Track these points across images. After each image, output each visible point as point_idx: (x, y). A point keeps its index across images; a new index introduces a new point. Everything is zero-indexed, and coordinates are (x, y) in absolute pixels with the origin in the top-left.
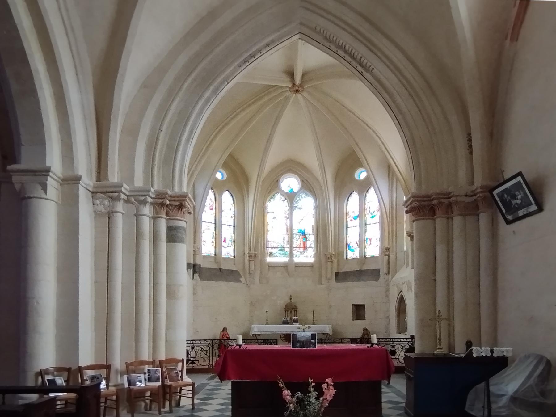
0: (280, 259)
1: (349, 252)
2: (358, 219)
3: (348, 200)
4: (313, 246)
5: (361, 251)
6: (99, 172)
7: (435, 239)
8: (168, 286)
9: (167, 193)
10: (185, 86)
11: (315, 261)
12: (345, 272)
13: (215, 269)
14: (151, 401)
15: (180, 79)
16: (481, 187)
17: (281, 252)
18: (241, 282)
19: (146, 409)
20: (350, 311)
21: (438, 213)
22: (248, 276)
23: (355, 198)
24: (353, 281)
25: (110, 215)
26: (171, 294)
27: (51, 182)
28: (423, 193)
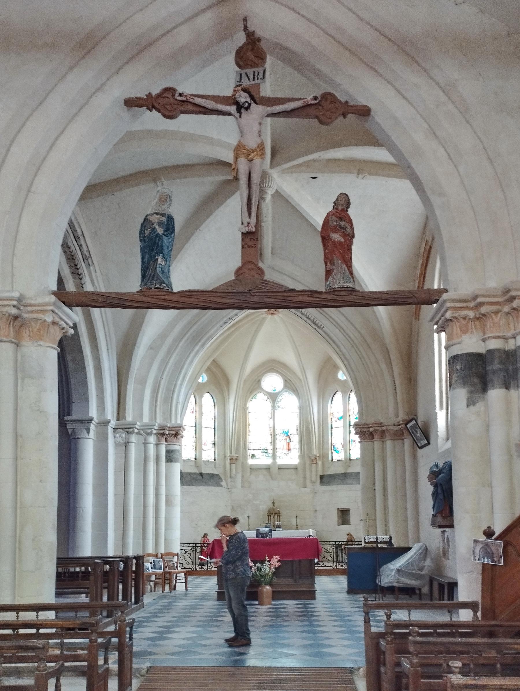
0: (264, 460)
1: (334, 453)
2: (342, 420)
3: (332, 400)
4: (298, 446)
5: (345, 452)
6: (118, 413)
7: (374, 456)
8: (167, 496)
10: (180, 345)
11: (300, 463)
13: (195, 474)
14: (156, 584)
17: (264, 454)
18: (221, 486)
19: (151, 591)
20: (335, 516)
21: (376, 437)
22: (229, 480)
23: (339, 396)
24: (338, 485)
25: (126, 444)
26: (169, 502)
27: (92, 427)
28: (363, 422)
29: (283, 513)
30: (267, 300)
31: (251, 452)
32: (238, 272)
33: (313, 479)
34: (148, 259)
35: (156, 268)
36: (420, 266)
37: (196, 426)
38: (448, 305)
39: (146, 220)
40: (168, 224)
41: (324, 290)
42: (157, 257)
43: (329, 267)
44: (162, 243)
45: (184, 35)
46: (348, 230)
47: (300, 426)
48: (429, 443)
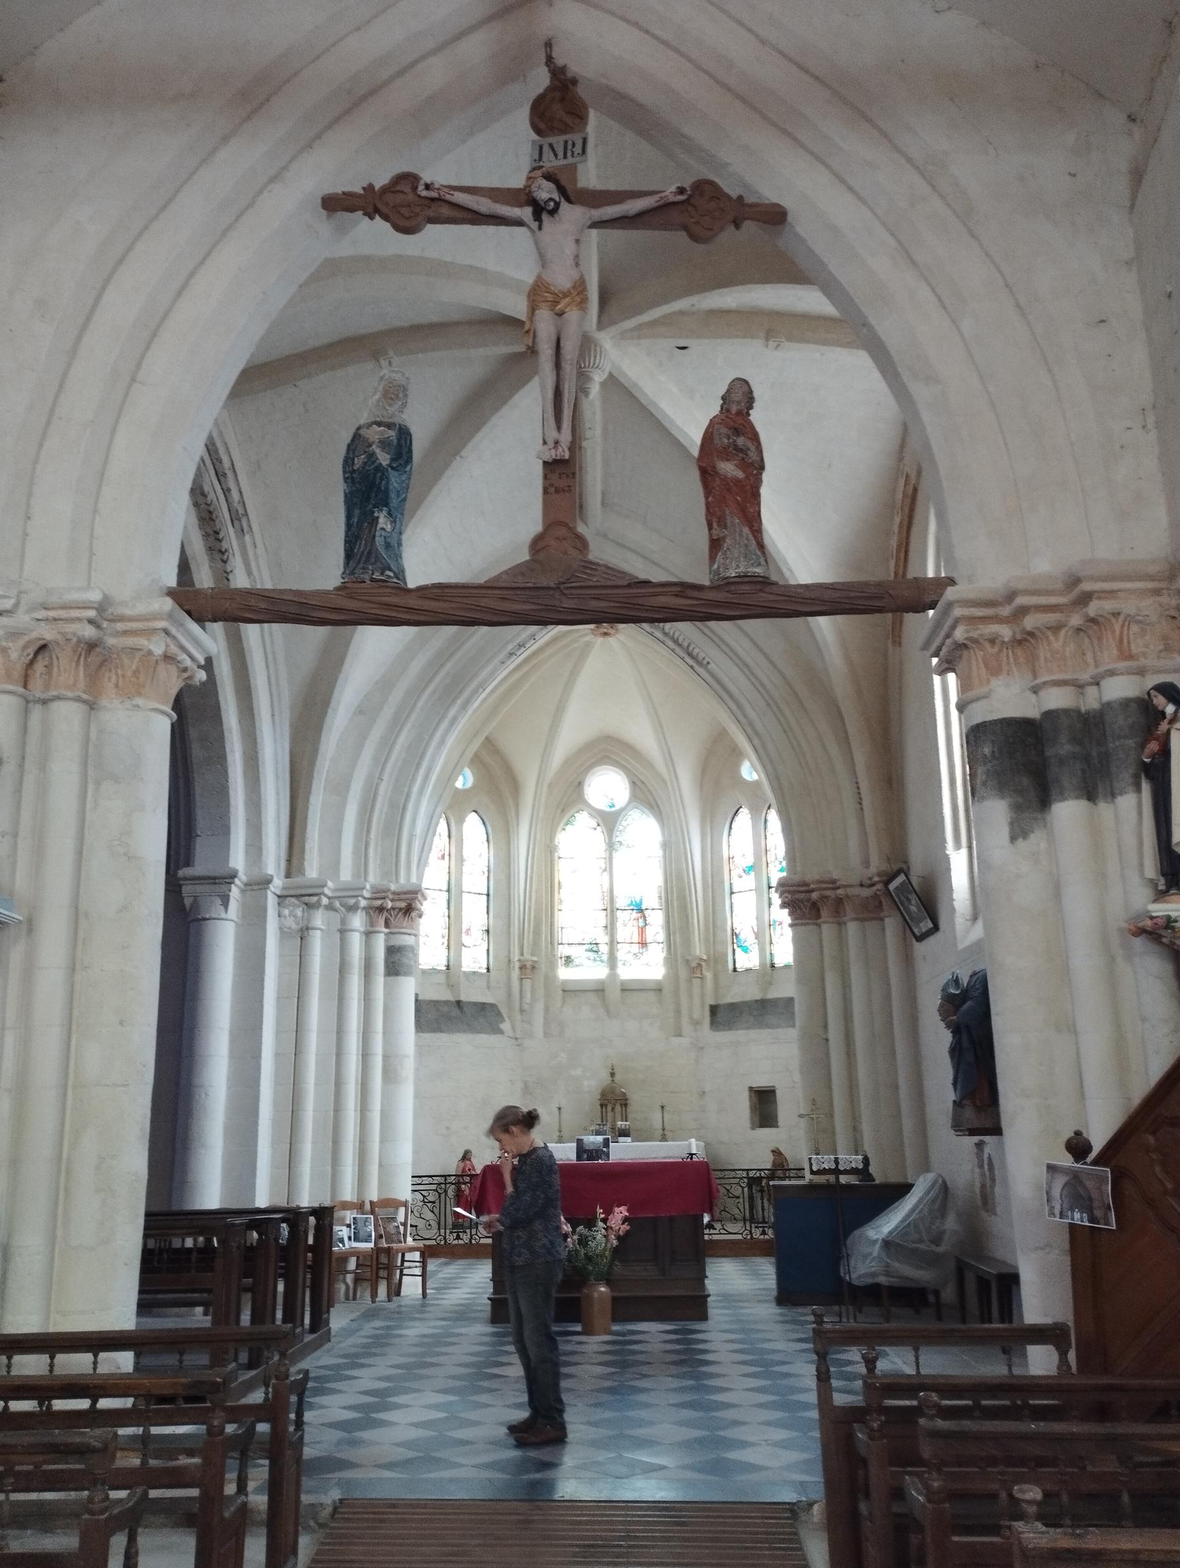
3: (730, 828)
4: (661, 937)
5: (762, 950)
8: (386, 1058)
9: (389, 890)
10: (420, 704)
11: (666, 976)
12: (731, 1005)
13: (447, 1002)
14: (357, 1280)
15: (414, 694)
16: (879, 875)
17: (592, 955)
18: (501, 1032)
20: (743, 1105)
22: (518, 1017)
24: (748, 1028)
25: (304, 933)
27: (235, 892)
28: (797, 878)
29: (634, 1098)
30: (594, 604)
31: (563, 951)
32: (537, 544)
33: (696, 1015)
34: (359, 520)
35: (374, 537)
36: (896, 529)
37: (448, 891)
38: (958, 612)
39: (357, 436)
40: (399, 445)
41: (707, 583)
42: (376, 514)
43: (717, 532)
44: (387, 483)
45: (436, 74)
46: (751, 454)
47: (666, 889)
48: (936, 928)
